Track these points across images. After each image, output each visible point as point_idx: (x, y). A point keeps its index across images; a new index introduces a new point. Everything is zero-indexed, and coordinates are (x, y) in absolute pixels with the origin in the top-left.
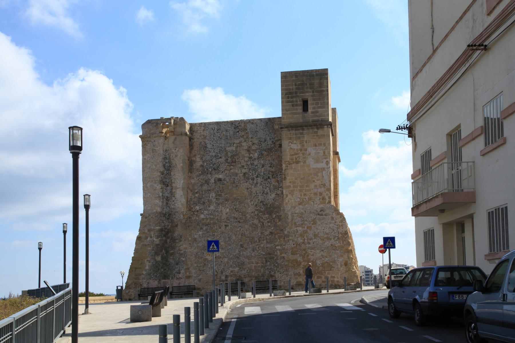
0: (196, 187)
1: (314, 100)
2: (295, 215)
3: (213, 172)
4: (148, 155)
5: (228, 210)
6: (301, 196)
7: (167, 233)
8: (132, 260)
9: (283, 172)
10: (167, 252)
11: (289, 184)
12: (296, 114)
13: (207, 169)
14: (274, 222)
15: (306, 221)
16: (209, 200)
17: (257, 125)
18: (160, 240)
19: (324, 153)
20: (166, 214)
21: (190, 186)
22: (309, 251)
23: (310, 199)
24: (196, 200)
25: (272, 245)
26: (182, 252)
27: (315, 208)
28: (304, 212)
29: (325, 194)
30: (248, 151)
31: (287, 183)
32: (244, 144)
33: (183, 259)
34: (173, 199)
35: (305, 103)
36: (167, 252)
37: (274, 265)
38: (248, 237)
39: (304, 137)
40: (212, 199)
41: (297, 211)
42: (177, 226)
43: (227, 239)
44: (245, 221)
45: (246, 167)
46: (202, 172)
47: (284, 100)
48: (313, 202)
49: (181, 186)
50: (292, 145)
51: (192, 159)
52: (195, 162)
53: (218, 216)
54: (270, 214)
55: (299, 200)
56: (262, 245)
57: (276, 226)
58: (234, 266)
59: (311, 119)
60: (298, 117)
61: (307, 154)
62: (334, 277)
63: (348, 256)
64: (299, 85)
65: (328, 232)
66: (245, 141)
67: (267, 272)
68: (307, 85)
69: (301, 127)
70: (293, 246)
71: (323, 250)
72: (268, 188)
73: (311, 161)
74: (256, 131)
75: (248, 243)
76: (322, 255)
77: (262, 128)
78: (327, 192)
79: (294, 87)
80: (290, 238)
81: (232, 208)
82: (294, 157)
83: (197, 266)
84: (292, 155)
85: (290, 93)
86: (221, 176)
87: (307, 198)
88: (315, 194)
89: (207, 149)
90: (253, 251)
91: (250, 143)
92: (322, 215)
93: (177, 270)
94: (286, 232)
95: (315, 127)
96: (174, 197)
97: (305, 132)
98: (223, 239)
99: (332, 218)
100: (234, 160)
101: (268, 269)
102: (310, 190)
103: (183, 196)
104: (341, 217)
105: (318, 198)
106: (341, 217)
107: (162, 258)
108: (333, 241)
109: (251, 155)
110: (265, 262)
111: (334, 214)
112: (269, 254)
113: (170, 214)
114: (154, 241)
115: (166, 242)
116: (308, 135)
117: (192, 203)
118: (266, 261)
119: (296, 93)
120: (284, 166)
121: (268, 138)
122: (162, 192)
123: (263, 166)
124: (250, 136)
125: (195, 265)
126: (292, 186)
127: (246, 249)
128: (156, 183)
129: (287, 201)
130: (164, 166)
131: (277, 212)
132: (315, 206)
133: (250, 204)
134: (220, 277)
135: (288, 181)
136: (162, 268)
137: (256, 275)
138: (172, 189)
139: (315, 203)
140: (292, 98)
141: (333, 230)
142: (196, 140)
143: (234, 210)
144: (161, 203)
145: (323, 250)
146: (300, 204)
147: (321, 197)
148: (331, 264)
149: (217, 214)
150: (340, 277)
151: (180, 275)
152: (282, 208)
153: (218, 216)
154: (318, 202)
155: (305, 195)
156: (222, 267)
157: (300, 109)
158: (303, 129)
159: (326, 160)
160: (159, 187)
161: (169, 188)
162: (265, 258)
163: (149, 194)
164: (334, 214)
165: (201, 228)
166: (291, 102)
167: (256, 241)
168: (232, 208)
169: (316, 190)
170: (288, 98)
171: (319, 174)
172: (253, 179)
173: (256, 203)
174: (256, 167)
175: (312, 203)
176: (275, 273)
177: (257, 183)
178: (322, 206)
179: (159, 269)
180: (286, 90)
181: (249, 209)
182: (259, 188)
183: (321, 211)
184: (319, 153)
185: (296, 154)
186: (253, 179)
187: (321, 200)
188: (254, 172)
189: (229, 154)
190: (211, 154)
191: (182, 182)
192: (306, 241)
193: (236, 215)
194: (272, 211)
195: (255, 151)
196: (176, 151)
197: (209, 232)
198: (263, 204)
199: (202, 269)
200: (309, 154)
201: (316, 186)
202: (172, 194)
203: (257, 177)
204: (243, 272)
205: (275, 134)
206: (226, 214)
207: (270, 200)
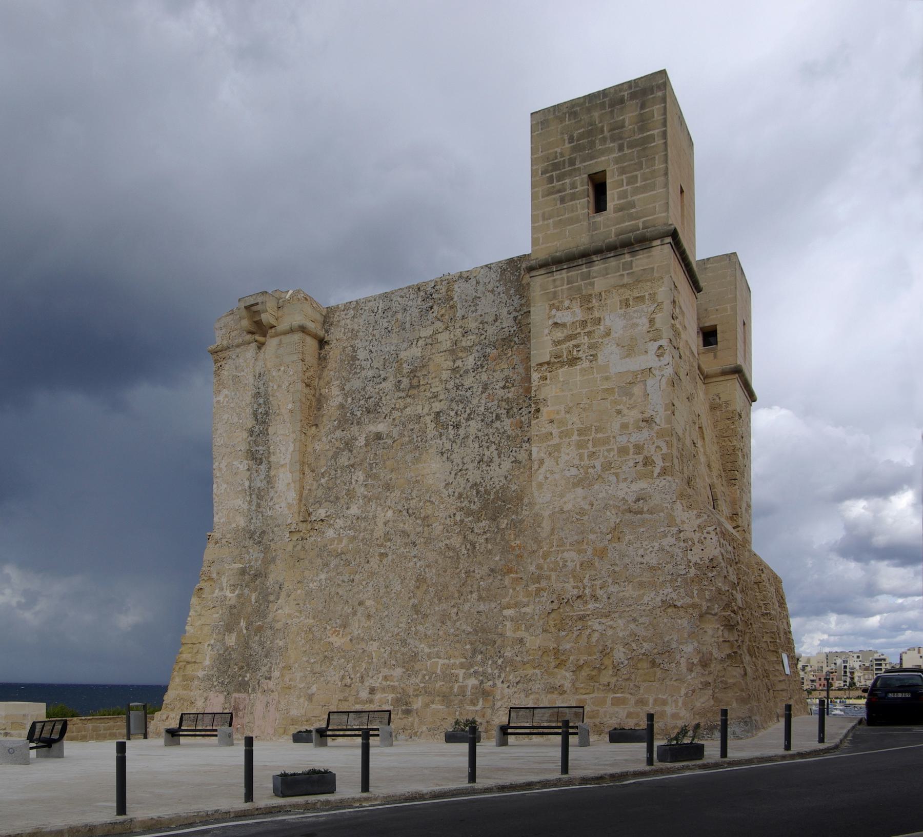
1: (622, 171)
4: (225, 391)
5: (390, 513)
6: (581, 459)
12: (571, 221)
13: (352, 414)
14: (503, 539)
19: (652, 321)
20: (254, 532)
23: (607, 466)
24: (320, 493)
25: (493, 605)
27: (621, 494)
28: (587, 507)
29: (653, 448)
30: (452, 352)
31: (540, 426)
33: (281, 643)
35: (599, 187)
42: (273, 560)
49: (287, 461)
50: (559, 314)
51: (323, 391)
53: (365, 530)
56: (466, 607)
58: (393, 662)
62: (664, 703)
64: (581, 136)
68: (602, 131)
71: (635, 620)
73: (610, 354)
75: (431, 602)
76: (632, 634)
85: (556, 167)
86: (381, 427)
88: (623, 451)
89: (357, 362)
91: (459, 332)
93: (264, 669)
102: (606, 441)
105: (631, 463)
109: (459, 363)
111: (678, 505)
113: (264, 532)
117: (311, 501)
118: (474, 652)
119: (572, 162)
122: (250, 479)
124: (459, 314)
126: (555, 432)
127: (425, 616)
129: (541, 477)
130: (255, 414)
132: (623, 485)
134: (358, 692)
137: (444, 689)
138: (269, 468)
139: (622, 476)
142: (334, 344)
143: (405, 512)
144: (245, 506)
146: (575, 485)
147: (640, 458)
151: (271, 684)
152: (526, 501)
153: (365, 530)
156: (364, 665)
157: (583, 204)
161: (263, 467)
164: (678, 505)
165: (326, 565)
166: (559, 191)
168: (400, 507)
174: (469, 393)
177: (467, 437)
183: (638, 500)
185: (570, 338)
186: (457, 426)
187: (640, 467)
191: (291, 449)
192: (587, 591)
193: (408, 525)
194: (496, 507)
197: (341, 574)
198: (478, 492)
199: (317, 668)
200: (608, 334)
201: (624, 426)
202: (269, 480)
203: (468, 420)
204: (413, 680)
206: (385, 524)
207: (496, 480)
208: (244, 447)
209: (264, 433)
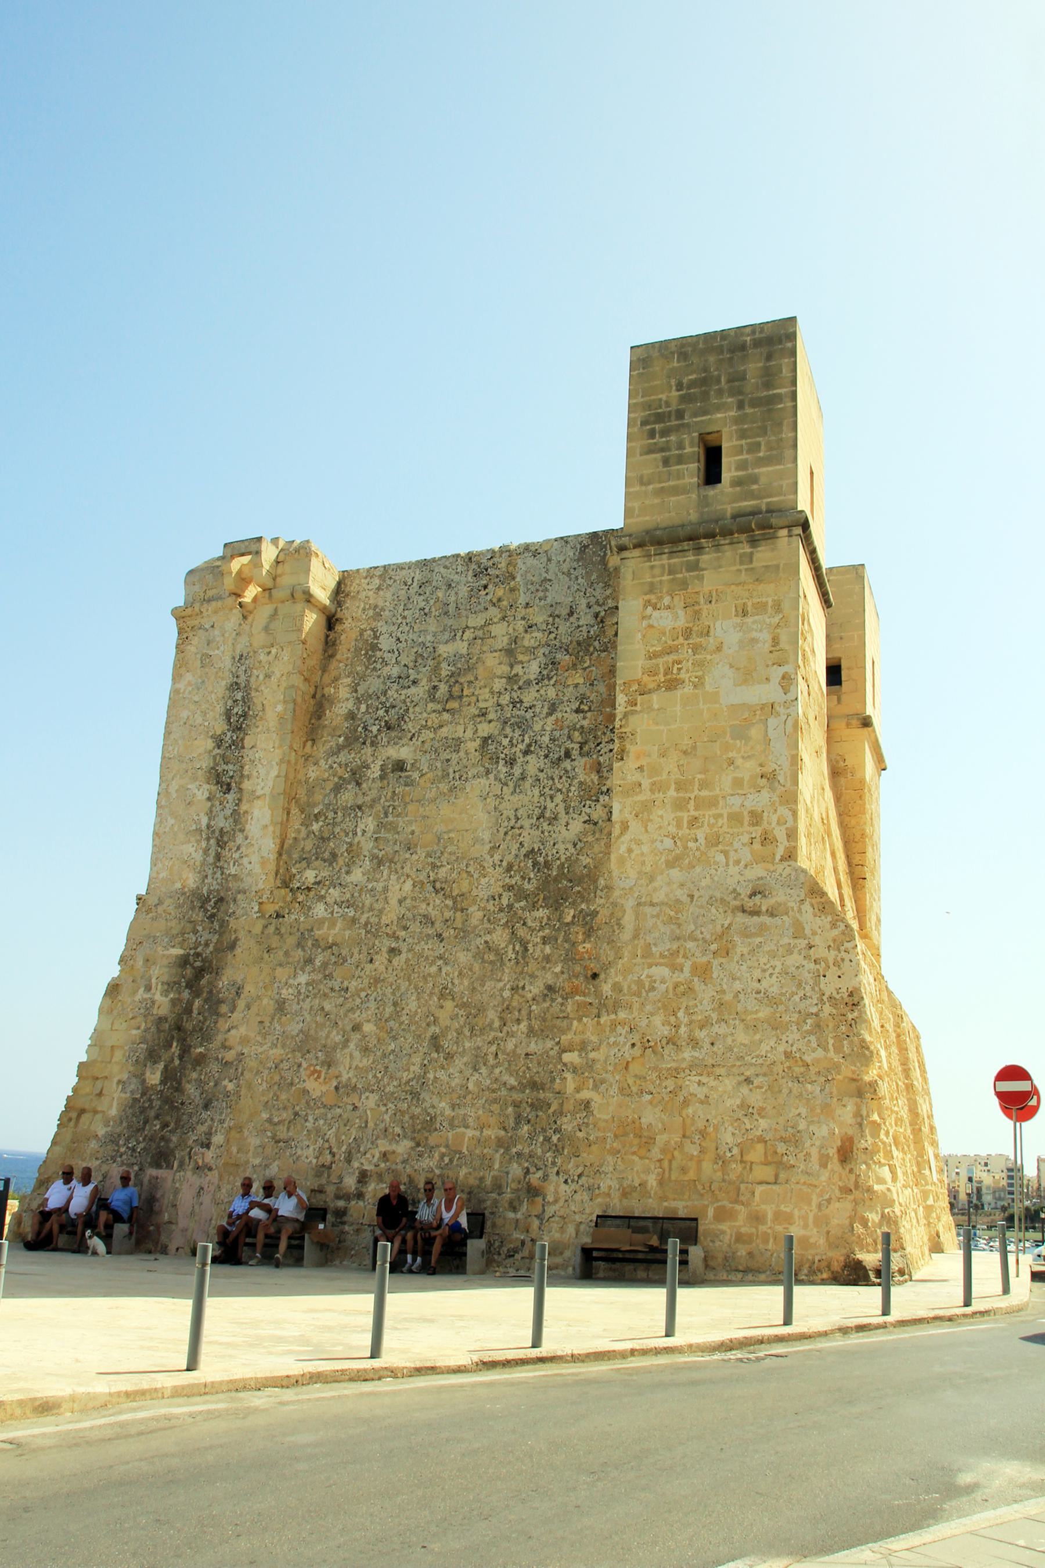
0: (318, 797)
2: (648, 910)
3: (384, 737)
6: (679, 826)
7: (200, 973)
8: (79, 1075)
9: (617, 724)
10: (185, 1050)
11: (637, 777)
12: (675, 491)
13: (365, 728)
14: (566, 940)
15: (692, 938)
16: (351, 844)
17: (549, 560)
18: (172, 1001)
19: (775, 641)
20: (208, 899)
21: (302, 793)
22: (691, 1084)
23: (714, 841)
25: (550, 1044)
26: (230, 1055)
29: (774, 818)
30: (510, 652)
31: (624, 773)
32: (499, 630)
33: (230, 1086)
34: (239, 838)
36: (185, 1050)
37: (548, 1139)
38: (464, 1005)
39: (701, 578)
40: (363, 844)
41: (660, 896)
43: (389, 1010)
44: (464, 933)
45: (491, 716)
46: (346, 739)
47: (637, 445)
48: (726, 853)
49: (267, 790)
52: (331, 701)
54: (556, 903)
55: (668, 843)
57: (571, 957)
58: (398, 1130)
59: (729, 509)
60: (684, 502)
61: (712, 647)
63: (858, 1114)
64: (692, 384)
65: (774, 990)
66: (503, 619)
67: (516, 1170)
68: (719, 381)
69: (690, 539)
70: (628, 1053)
71: (748, 1081)
72: (559, 798)
74: (546, 580)
75: (459, 1032)
76: (744, 1105)
77: (565, 567)
78: (784, 811)
79: (675, 394)
80: (622, 1015)
81: (422, 877)
82: (660, 661)
83: (269, 1121)
84: (655, 655)
85: (660, 418)
87: (701, 835)
88: (735, 818)
89: (379, 654)
90: (475, 1069)
91: (520, 625)
92: (756, 913)
93: (202, 1129)
94: (606, 988)
95: (743, 537)
96: (242, 831)
97: (705, 558)
98: (372, 1005)
99: (798, 931)
100: (456, 689)
101: (519, 1155)
102: (713, 803)
103: (271, 829)
104: (834, 926)
105: (746, 839)
106: (834, 926)
107: (168, 1075)
108: (793, 1035)
109: (518, 669)
110: (511, 1122)
111: (806, 906)
112: (534, 1085)
113: (221, 900)
114: (153, 1002)
115: (188, 1010)
116: (719, 570)
117: (296, 856)
118: (518, 1119)
119: (680, 414)
120: (621, 699)
121: (583, 602)
123: (553, 709)
125: (265, 1116)
126: (646, 783)
127: (449, 1056)
128: (195, 779)
129: (623, 848)
130: (228, 714)
131: (583, 899)
132: (733, 870)
133: (488, 862)
134: (341, 1178)
135: (631, 763)
136: (157, 1117)
140: (665, 433)
141: (799, 985)
142: (348, 624)
144: (198, 857)
145: (748, 1081)
146: (670, 864)
148: (781, 1148)
149: (368, 901)
150: (817, 1222)
151: (209, 1155)
152: (602, 882)
154: (746, 855)
155: (694, 822)
156: (354, 1133)
157: (692, 471)
158: (699, 549)
159: (781, 670)
160: (201, 791)
161: (230, 797)
162: (516, 1105)
163: (171, 821)
164: (806, 906)
165: (309, 961)
166: (662, 450)
167: (490, 1025)
168: (422, 877)
169: (736, 801)
170: (652, 434)
171: (755, 732)
172: (511, 762)
173: (509, 858)
175: (721, 858)
176: (545, 1178)
178: (758, 871)
179: (146, 1122)
180: (648, 406)
181: (483, 881)
182: (531, 795)
183: (754, 894)
184: (754, 641)
185: (669, 651)
186: (511, 762)
187: (757, 846)
188: (518, 732)
189: (445, 670)
190: (386, 671)
191: (274, 773)
192: (683, 1030)
194: (561, 890)
195: (532, 651)
196: (271, 658)
199: (282, 1133)
200: (719, 649)
201: (738, 783)
202: (237, 817)
203: (526, 753)
205: (607, 585)
206: (400, 902)
208: (206, 763)
209: (238, 744)
